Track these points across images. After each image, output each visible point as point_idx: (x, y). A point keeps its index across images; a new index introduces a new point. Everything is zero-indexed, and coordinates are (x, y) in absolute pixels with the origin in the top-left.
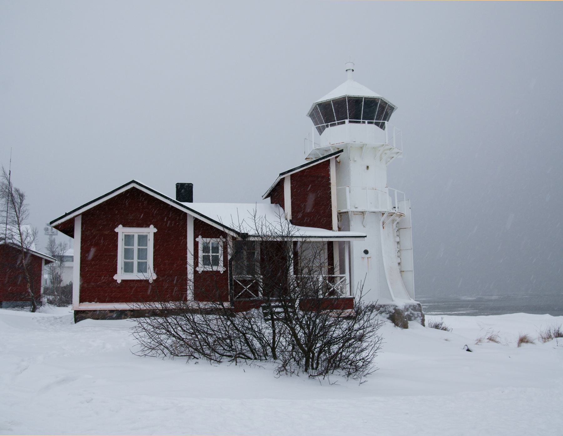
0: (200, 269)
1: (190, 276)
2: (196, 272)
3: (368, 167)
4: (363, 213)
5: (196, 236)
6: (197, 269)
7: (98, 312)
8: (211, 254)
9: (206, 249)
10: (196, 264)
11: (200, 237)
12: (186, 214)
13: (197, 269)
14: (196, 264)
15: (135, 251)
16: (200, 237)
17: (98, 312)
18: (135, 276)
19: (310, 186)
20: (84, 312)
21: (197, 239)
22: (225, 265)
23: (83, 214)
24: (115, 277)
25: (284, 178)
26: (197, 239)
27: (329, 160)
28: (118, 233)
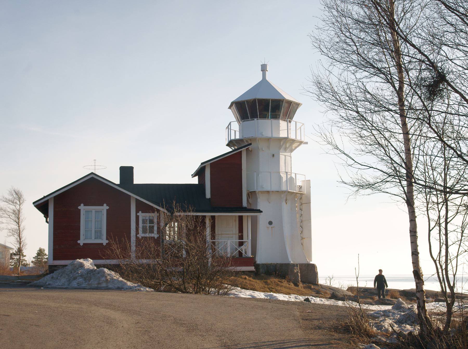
0: (141, 235)
1: (133, 239)
2: (137, 238)
3: (273, 155)
4: (268, 192)
5: (137, 212)
6: (138, 236)
7: (162, 288)
8: (148, 225)
9: (144, 221)
10: (137, 232)
11: (140, 212)
12: (130, 196)
13: (138, 236)
14: (137, 232)
15: (93, 222)
16: (140, 212)
17: (162, 288)
19: (208, 195)
20: (56, 266)
21: (138, 214)
22: (158, 232)
23: (55, 197)
25: (205, 166)
26: (138, 214)
27: (241, 151)
28: (80, 210)
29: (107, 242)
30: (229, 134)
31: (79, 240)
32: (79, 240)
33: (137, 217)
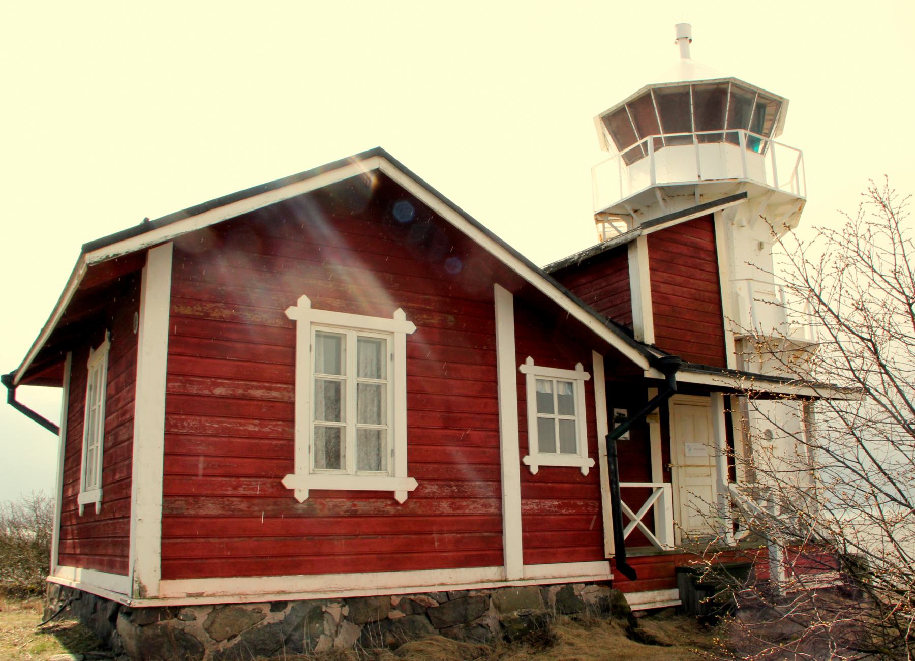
0: (536, 460)
2: (525, 469)
6: (527, 460)
9: (544, 402)
10: (524, 449)
11: (530, 360)
14: (524, 449)
16: (530, 360)
18: (350, 478)
21: (523, 368)
24: (288, 481)
26: (523, 368)
27: (712, 215)
29: (413, 484)
30: (633, 604)
31: (536, 364)
32: (536, 364)
33: (521, 380)
